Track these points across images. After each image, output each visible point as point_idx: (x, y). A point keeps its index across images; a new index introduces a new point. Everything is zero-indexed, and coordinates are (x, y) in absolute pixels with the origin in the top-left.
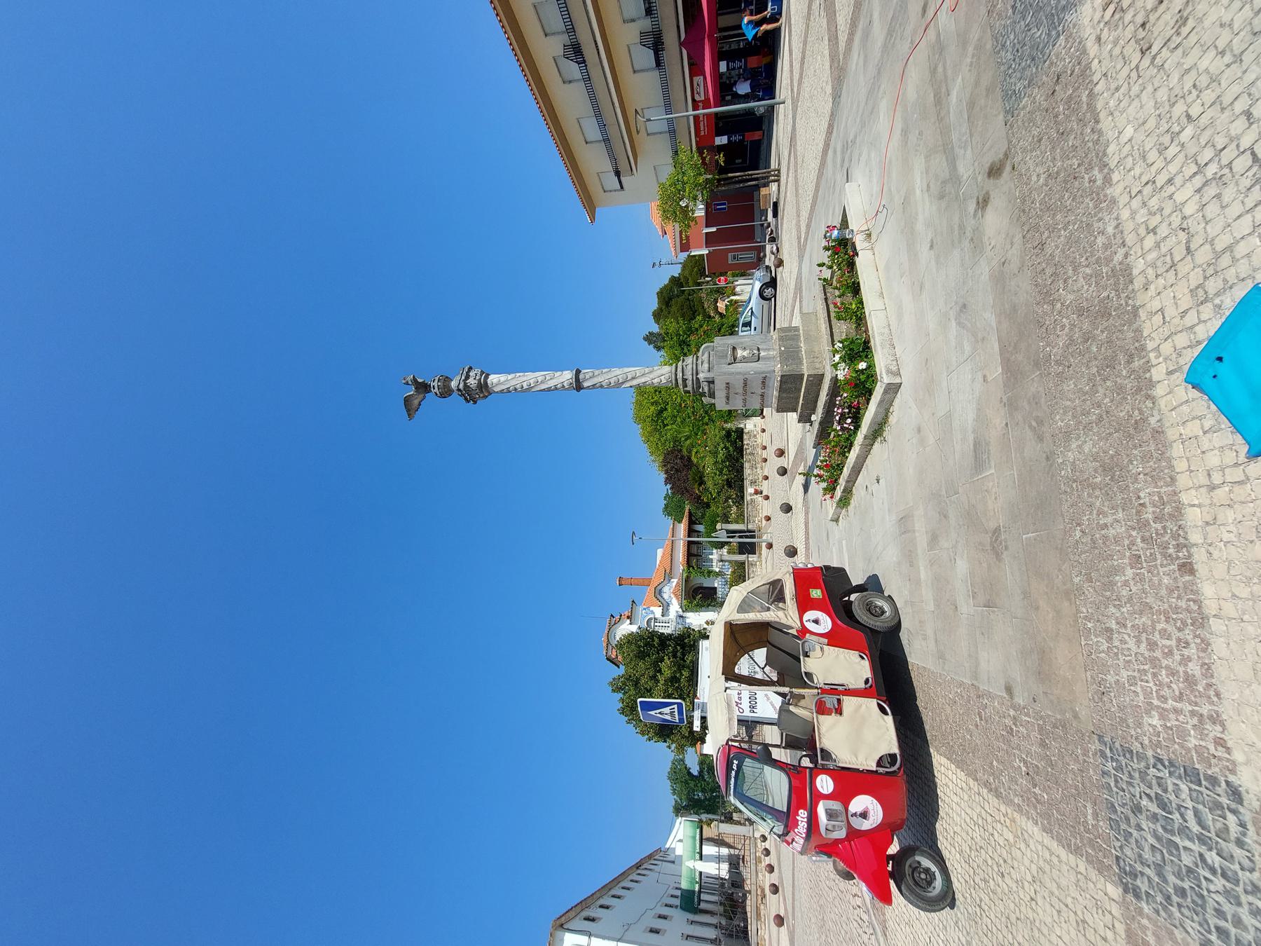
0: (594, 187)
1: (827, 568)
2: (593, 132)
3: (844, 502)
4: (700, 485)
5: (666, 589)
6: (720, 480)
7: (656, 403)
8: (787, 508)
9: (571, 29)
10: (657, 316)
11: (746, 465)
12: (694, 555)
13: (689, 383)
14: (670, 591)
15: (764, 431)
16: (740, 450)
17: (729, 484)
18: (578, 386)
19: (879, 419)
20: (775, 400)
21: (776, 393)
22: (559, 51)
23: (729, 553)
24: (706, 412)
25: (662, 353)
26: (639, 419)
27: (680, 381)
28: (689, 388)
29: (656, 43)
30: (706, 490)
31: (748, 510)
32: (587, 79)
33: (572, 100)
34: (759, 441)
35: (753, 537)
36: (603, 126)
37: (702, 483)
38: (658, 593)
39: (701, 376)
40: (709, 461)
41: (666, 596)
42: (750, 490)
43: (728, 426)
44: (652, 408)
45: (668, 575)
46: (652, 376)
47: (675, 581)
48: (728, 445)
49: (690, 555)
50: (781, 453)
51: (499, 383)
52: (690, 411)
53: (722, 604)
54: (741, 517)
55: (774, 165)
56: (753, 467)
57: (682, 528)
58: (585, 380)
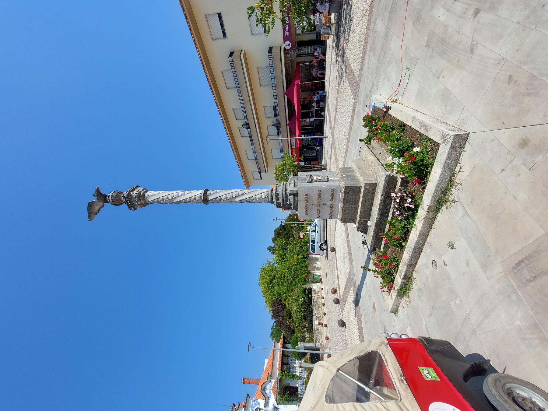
0: (250, 177)
1: (429, 341)
2: (251, 155)
3: (404, 290)
4: (290, 318)
5: (268, 387)
6: (300, 315)
7: (270, 275)
8: (342, 324)
9: (246, 118)
10: (274, 240)
11: (314, 308)
12: (285, 364)
13: (280, 197)
14: (271, 388)
15: (322, 289)
16: (311, 300)
17: (305, 318)
18: (205, 200)
19: (444, 185)
20: (340, 212)
21: (341, 205)
22: (241, 125)
23: (305, 362)
24: (294, 280)
25: (274, 256)
26: (262, 284)
27: (274, 196)
28: (280, 201)
29: (278, 125)
30: (293, 321)
31: (315, 334)
32: (251, 136)
33: (244, 143)
34: (320, 295)
35: (318, 350)
36: (255, 153)
37: (290, 317)
38: (263, 389)
39: (288, 192)
40: (295, 304)
41: (267, 392)
42: (316, 322)
43: (304, 286)
44: (268, 278)
45: (270, 377)
46: (255, 193)
47: (273, 381)
48: (304, 296)
49: (283, 364)
50: (335, 291)
51: (153, 195)
52: (286, 279)
53: (301, 399)
54: (311, 340)
55: (323, 163)
56: (317, 309)
57: (279, 345)
58: (210, 194)
